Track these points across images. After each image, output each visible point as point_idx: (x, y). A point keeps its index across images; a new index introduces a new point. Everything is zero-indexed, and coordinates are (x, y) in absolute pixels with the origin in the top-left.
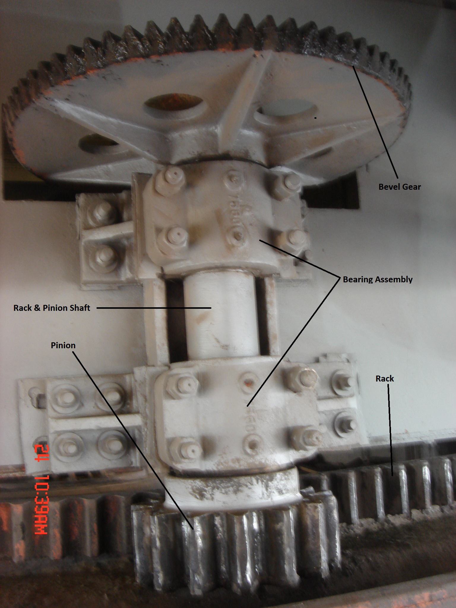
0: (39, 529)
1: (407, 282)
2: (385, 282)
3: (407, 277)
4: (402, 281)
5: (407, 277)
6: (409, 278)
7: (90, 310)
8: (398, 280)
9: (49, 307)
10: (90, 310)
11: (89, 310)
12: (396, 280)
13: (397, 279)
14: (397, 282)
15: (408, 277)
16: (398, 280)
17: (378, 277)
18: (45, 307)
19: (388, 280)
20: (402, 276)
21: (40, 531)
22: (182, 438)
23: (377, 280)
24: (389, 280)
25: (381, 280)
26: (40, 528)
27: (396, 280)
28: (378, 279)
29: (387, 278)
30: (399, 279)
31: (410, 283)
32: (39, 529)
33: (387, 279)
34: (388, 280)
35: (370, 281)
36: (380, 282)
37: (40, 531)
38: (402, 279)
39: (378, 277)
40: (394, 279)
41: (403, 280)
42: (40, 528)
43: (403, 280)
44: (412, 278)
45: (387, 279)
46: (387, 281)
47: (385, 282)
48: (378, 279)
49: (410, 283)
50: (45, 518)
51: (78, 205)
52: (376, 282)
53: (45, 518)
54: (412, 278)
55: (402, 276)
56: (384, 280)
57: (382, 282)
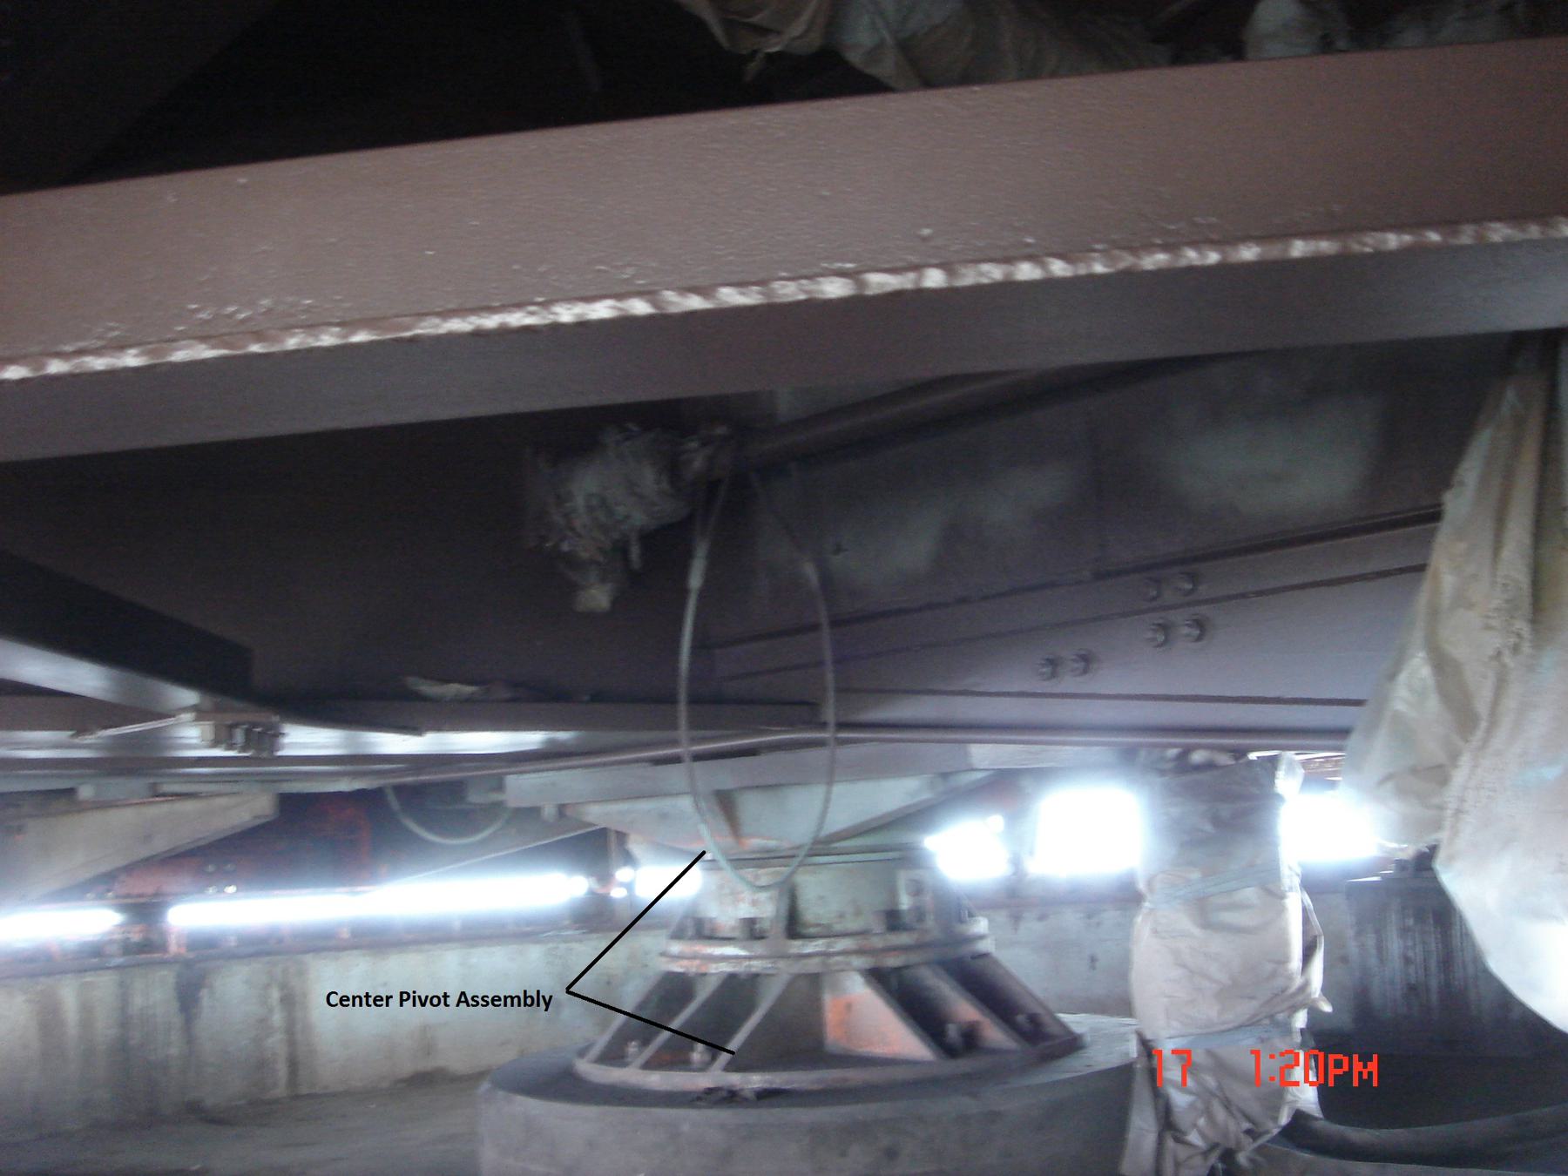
0: (1365, 1077)
1: (538, 1005)
2: (483, 1005)
3: (538, 992)
4: (525, 1004)
5: (538, 992)
6: (544, 997)
7: (448, 1006)
8: (516, 1000)
9: (414, 997)
10: (448, 1006)
11: (446, 1005)
12: (509, 1000)
13: (512, 998)
14: (512, 1005)
15: (541, 995)
16: (516, 1000)
17: (463, 994)
18: (405, 996)
19: (489, 1000)
20: (525, 992)
21: (1370, 1074)
22: (1440, 983)
23: (459, 1001)
24: (493, 1000)
25: (471, 1002)
26: (1361, 1073)
27: (509, 1000)
28: (463, 999)
29: (487, 997)
30: (518, 997)
31: (546, 1010)
32: (1365, 1077)
33: (486, 999)
34: (489, 1000)
35: (463, 998)
36: (468, 1005)
37: (1370, 1074)
38: (526, 997)
39: (463, 994)
40: (506, 998)
41: (529, 1001)
42: (1361, 1073)
43: (529, 1001)
44: (551, 997)
45: (486, 999)
46: (488, 1004)
47: (483, 1005)
48: (463, 999)
49: (546, 1010)
50: (1342, 1068)
51: (1298, 875)
52: (458, 1005)
53: (1342, 1068)
54: (551, 997)
55: (525, 992)
56: (479, 1000)
57: (473, 1006)
